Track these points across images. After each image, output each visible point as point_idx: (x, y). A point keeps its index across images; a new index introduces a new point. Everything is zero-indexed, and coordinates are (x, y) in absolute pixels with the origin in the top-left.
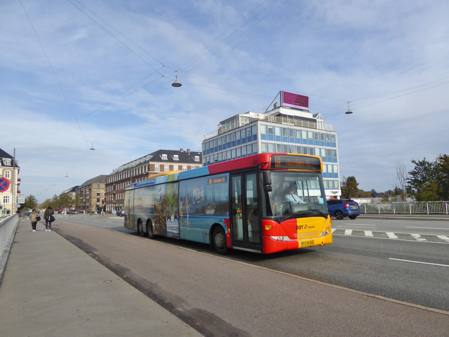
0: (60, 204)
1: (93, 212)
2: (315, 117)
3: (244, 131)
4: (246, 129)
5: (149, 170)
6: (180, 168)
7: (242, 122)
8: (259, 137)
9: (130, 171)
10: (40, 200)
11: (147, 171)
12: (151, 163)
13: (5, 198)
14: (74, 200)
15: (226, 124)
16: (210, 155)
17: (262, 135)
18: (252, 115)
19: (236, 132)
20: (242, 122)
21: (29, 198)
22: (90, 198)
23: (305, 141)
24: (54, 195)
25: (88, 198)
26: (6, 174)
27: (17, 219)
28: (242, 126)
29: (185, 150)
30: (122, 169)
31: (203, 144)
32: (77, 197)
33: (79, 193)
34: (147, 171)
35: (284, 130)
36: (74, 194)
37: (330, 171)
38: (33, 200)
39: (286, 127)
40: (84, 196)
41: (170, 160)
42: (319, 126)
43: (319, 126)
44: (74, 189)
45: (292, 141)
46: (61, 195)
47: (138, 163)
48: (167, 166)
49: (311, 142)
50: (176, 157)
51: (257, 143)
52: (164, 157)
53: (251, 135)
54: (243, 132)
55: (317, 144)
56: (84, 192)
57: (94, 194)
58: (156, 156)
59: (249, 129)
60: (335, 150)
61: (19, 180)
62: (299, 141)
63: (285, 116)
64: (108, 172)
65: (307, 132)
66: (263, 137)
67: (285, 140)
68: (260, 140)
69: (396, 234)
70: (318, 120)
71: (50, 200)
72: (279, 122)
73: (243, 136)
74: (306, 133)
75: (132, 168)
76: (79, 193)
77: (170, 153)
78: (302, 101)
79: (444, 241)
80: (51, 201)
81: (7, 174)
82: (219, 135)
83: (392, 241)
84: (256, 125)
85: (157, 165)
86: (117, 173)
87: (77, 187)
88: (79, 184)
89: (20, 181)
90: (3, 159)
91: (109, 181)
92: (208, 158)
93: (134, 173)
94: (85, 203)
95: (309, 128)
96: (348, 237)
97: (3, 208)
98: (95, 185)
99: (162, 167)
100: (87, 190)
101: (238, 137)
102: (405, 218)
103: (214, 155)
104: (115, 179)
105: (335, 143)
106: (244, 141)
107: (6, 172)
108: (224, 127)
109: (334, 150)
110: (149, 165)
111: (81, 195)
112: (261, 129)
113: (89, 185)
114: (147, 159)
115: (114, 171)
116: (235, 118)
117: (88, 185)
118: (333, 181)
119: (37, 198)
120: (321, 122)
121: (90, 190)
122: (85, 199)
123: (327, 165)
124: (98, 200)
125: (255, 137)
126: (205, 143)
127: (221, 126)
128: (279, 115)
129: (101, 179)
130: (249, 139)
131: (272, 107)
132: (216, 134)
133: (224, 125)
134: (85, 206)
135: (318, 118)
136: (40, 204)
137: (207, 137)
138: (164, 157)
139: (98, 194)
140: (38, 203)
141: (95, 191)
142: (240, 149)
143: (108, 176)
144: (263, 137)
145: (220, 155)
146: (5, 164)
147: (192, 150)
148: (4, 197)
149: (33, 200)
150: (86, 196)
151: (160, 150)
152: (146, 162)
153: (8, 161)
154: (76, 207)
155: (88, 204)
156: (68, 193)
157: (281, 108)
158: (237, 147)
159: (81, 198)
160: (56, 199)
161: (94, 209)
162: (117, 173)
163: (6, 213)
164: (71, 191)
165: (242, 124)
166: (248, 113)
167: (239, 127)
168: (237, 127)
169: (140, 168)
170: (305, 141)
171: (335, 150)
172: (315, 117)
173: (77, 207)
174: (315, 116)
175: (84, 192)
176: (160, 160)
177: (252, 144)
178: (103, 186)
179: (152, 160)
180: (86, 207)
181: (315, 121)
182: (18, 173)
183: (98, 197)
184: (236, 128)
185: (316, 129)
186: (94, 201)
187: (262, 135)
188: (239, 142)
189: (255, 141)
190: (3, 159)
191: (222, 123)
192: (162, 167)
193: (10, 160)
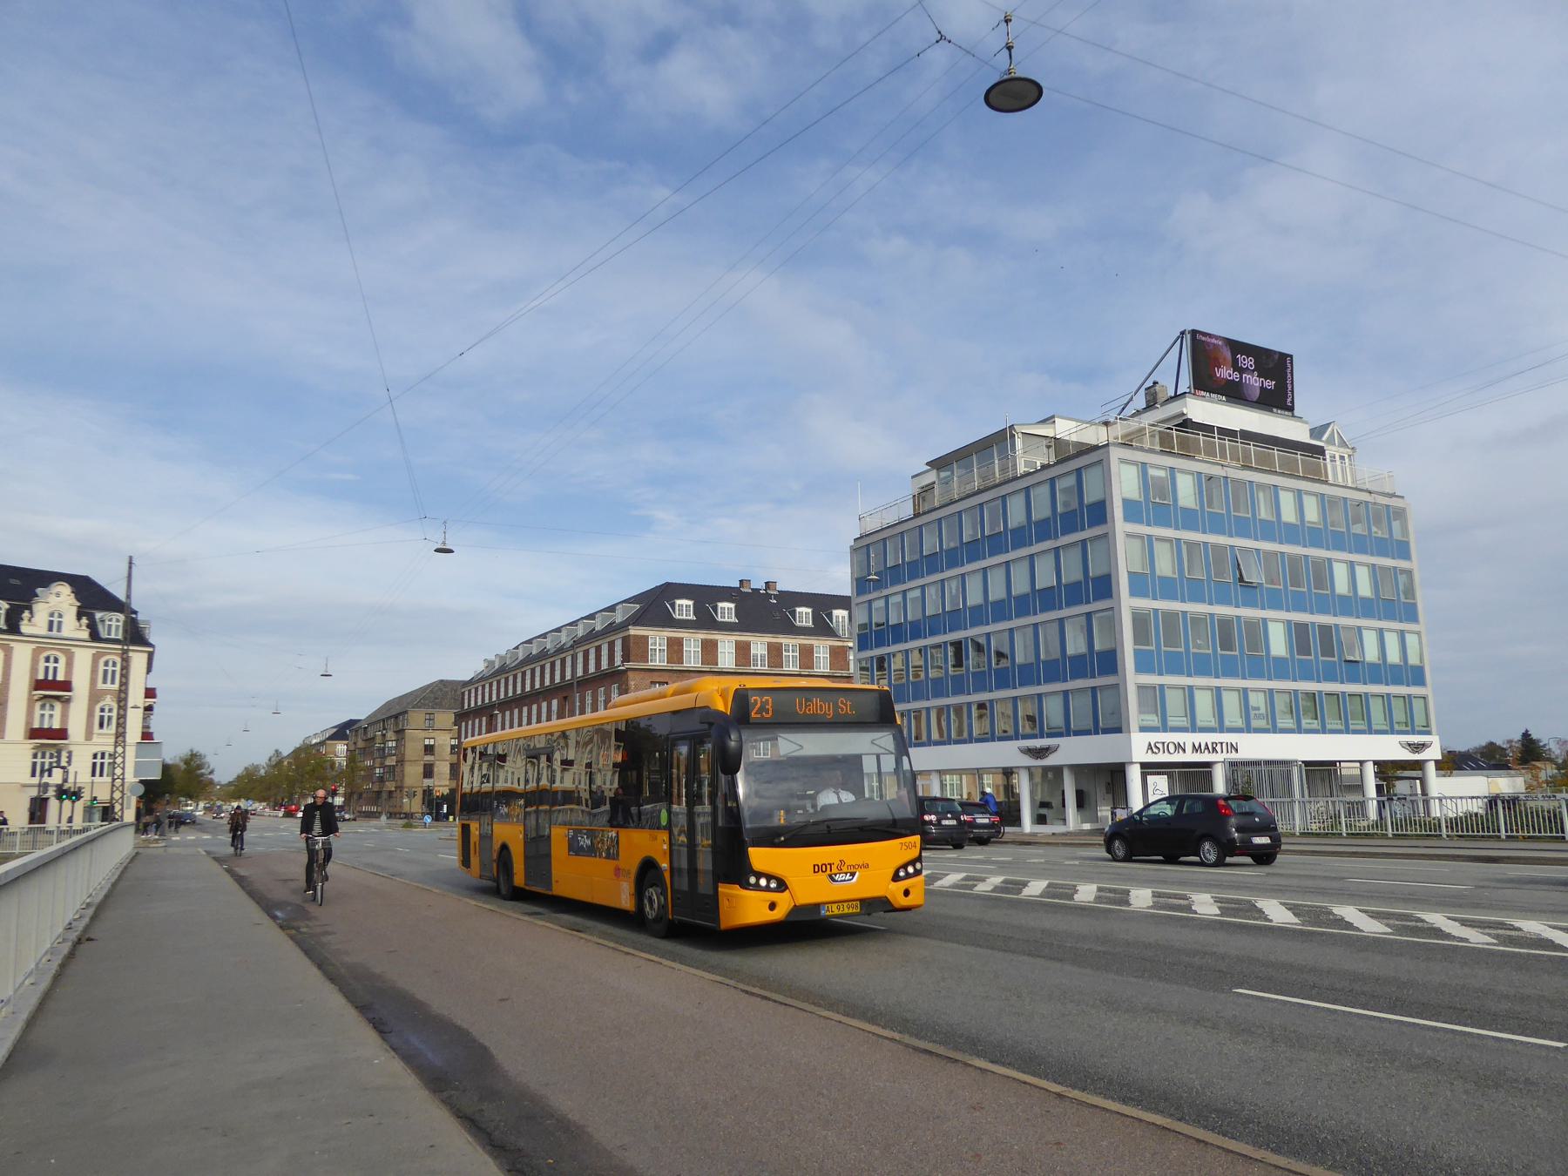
0: (292, 783)
1: (409, 816)
2: (1319, 438)
3: (1044, 490)
4: (1052, 480)
5: (626, 658)
6: (743, 651)
7: (1027, 458)
8: (1118, 511)
9: (499, 683)
10: (224, 770)
11: (618, 660)
12: (634, 631)
13: (99, 761)
14: (342, 772)
15: (957, 470)
16: (885, 592)
17: (1127, 503)
18: (1064, 429)
19: (1004, 497)
20: (1027, 458)
21: (187, 762)
22: (401, 762)
23: (1293, 533)
24: (272, 752)
25: (391, 761)
26: (106, 672)
27: (124, 844)
28: (1028, 474)
29: (758, 584)
30: (521, 655)
31: (854, 550)
32: (351, 757)
33: (361, 744)
34: (618, 660)
35: (1206, 483)
36: (341, 748)
37: (1393, 657)
38: (200, 767)
39: (1216, 471)
40: (376, 754)
41: (705, 620)
42: (1335, 474)
43: (1335, 474)
44: (342, 732)
45: (1243, 528)
46: (297, 751)
47: (581, 631)
48: (692, 643)
49: (1315, 536)
50: (726, 610)
51: (1107, 538)
52: (684, 607)
53: (1075, 505)
54: (1041, 495)
55: (1339, 542)
56: (379, 740)
57: (413, 749)
58: (654, 606)
59: (1070, 481)
60: (1409, 573)
61: (150, 693)
62: (1271, 530)
63: (1207, 429)
64: (464, 668)
65: (1299, 494)
66: (1133, 511)
67: (1216, 525)
68: (1121, 526)
69: (1293, 909)
70: (1330, 451)
71: (256, 768)
72: (1187, 452)
73: (1041, 511)
74: (1294, 501)
75: (561, 650)
76: (361, 744)
77: (705, 596)
78: (1269, 378)
79: (1437, 932)
80: (262, 772)
81: (110, 668)
82: (917, 515)
83: (1282, 932)
84: (1102, 463)
85: (657, 639)
86: (503, 670)
87: (351, 723)
88: (362, 713)
89: (154, 696)
90: (98, 615)
91: (471, 702)
92: (954, 586)
93: (528, 682)
94: (381, 780)
95: (1304, 478)
96: (1083, 910)
97: (86, 796)
98: (417, 718)
99: (675, 647)
100: (390, 735)
101: (1016, 516)
102: (1354, 849)
103: (904, 592)
104: (493, 694)
105: (1407, 543)
106: (1044, 530)
107: (106, 664)
108: (946, 482)
109: (1403, 571)
110: (626, 640)
111: (366, 752)
112: (1125, 483)
113: (396, 717)
114: (619, 617)
115: (490, 663)
116: (1000, 440)
117: (394, 716)
118: (1407, 700)
119: (212, 760)
120: (1342, 458)
121: (400, 732)
122: (382, 766)
123: (1381, 633)
124: (428, 772)
125: (1099, 513)
126: (864, 547)
127: (932, 477)
128: (1186, 424)
129: (439, 695)
130: (1070, 522)
131: (1140, 402)
132: (908, 511)
133: (943, 474)
134: (379, 793)
135: (1331, 441)
136: (224, 782)
137: (873, 524)
138: (684, 607)
139: (429, 749)
140: (216, 777)
141: (416, 738)
142: (979, 577)
143: (465, 684)
144: (1133, 511)
145: (932, 593)
146: (104, 635)
147: (783, 586)
148: (95, 756)
149: (200, 767)
150: (384, 757)
151: (668, 584)
152: (612, 628)
153: (114, 623)
154: (348, 797)
155: (390, 786)
156: (322, 743)
157: (1189, 400)
158: (1065, 540)
159: (368, 763)
160: (280, 762)
161: (415, 805)
162: (500, 671)
163: (97, 816)
164: (332, 737)
165: (1027, 464)
166: (1049, 420)
167: (1016, 478)
168: (1010, 475)
169: (558, 663)
170: (1293, 533)
171: (1409, 573)
172: (1319, 438)
173: (351, 794)
174: (1317, 432)
175: (379, 740)
176: (668, 621)
177: (1084, 542)
178: (446, 718)
179: (637, 620)
180: (384, 795)
181: (1320, 451)
182: (149, 670)
183: (429, 758)
184: (980, 492)
185: (1326, 482)
186: (412, 774)
187: (1127, 503)
188: (1020, 537)
189: (1097, 531)
190: (98, 615)
191: (938, 464)
192: (675, 647)
193: (122, 617)
